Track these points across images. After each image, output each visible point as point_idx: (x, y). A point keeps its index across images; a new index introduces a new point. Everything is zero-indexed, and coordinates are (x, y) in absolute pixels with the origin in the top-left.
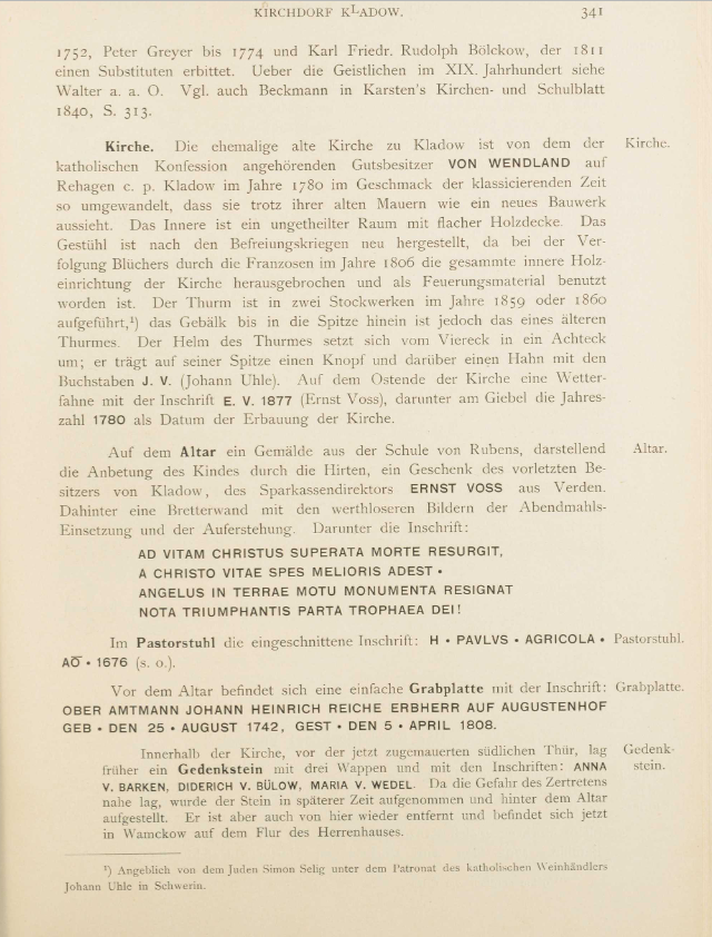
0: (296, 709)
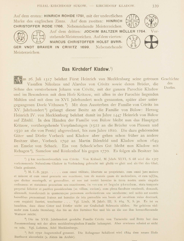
0: (54, 16)
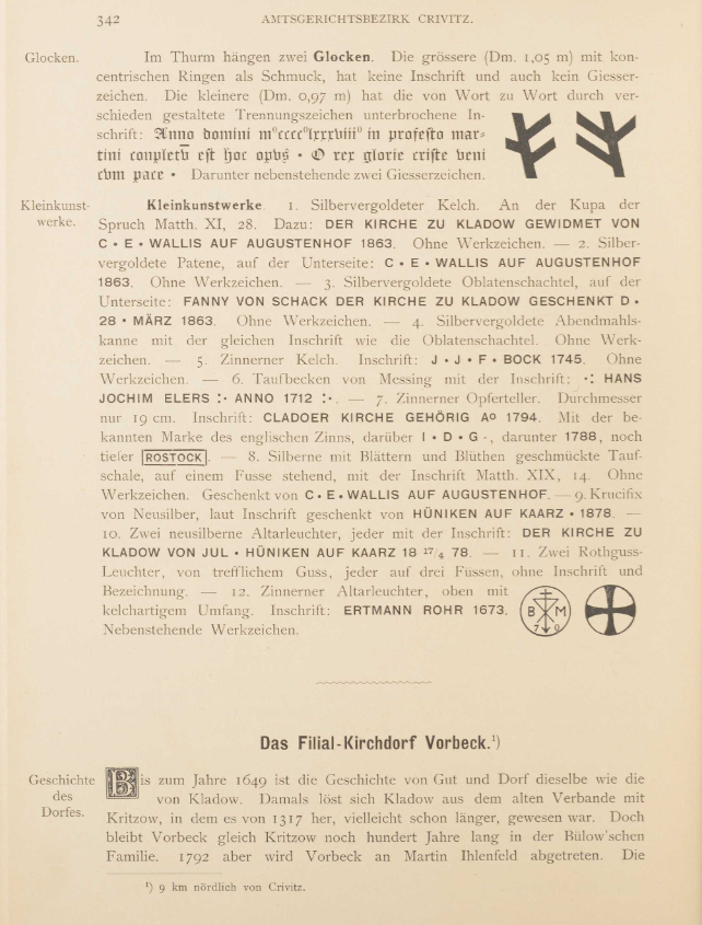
0: (455, 418)
